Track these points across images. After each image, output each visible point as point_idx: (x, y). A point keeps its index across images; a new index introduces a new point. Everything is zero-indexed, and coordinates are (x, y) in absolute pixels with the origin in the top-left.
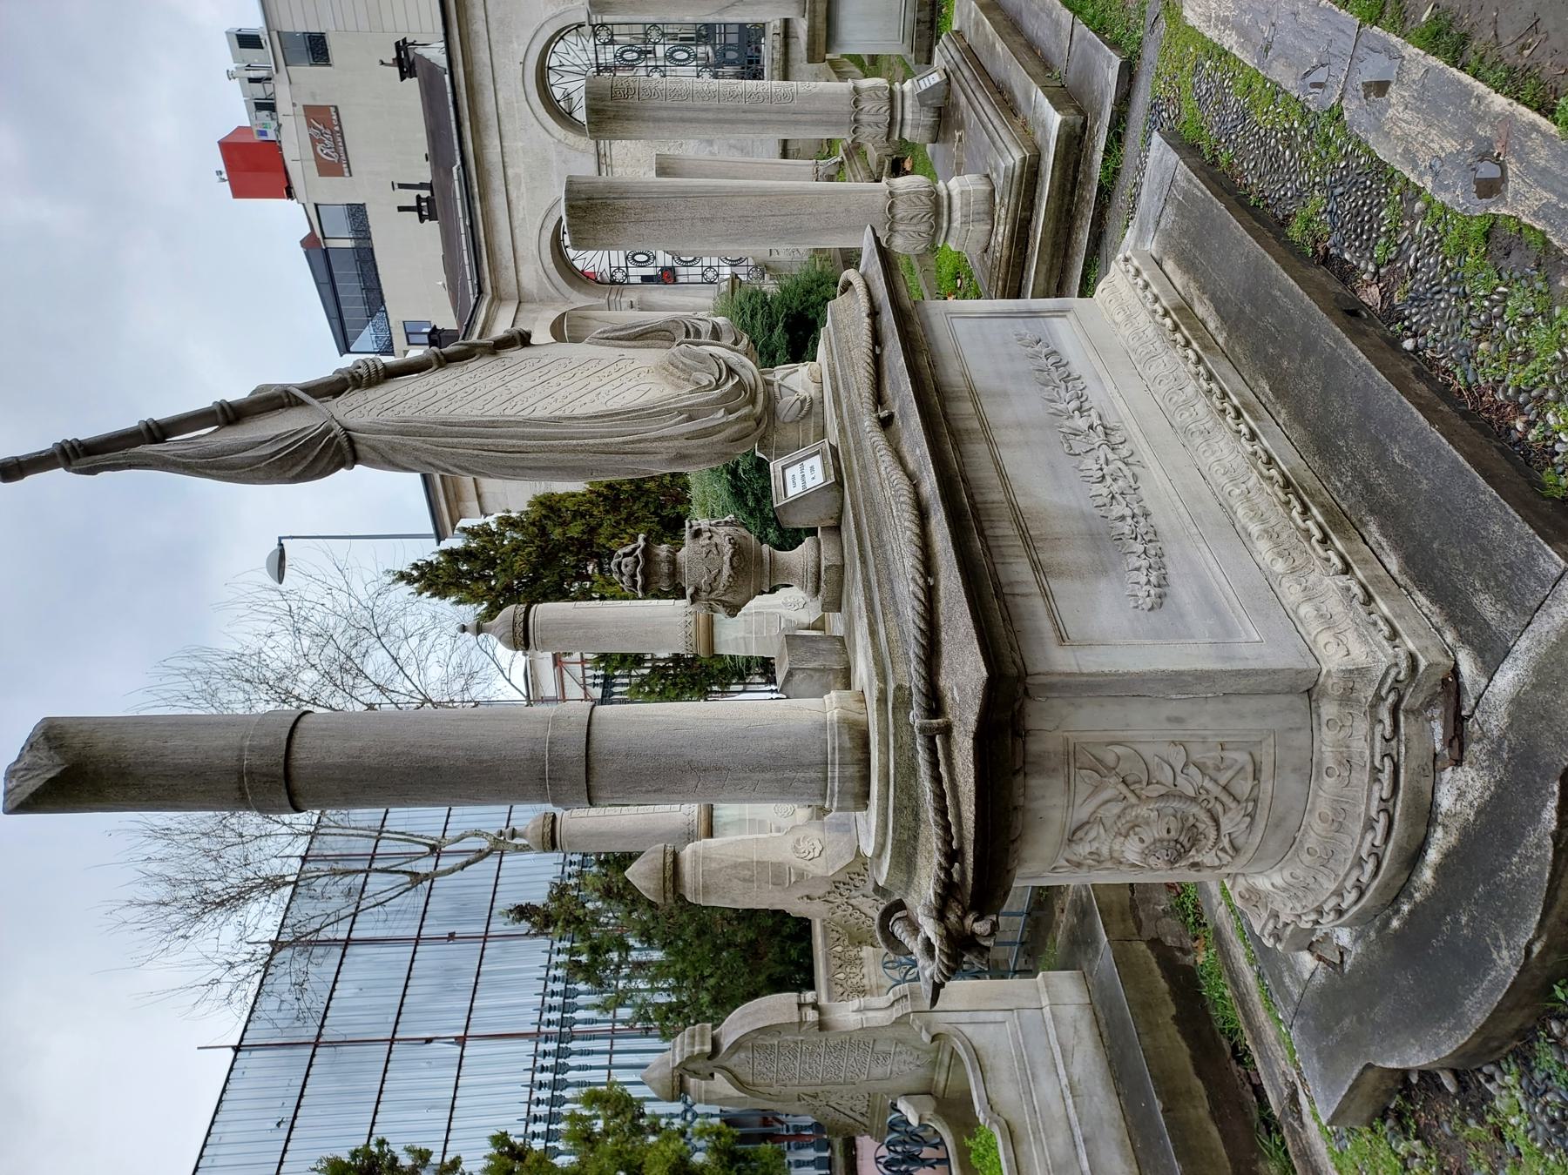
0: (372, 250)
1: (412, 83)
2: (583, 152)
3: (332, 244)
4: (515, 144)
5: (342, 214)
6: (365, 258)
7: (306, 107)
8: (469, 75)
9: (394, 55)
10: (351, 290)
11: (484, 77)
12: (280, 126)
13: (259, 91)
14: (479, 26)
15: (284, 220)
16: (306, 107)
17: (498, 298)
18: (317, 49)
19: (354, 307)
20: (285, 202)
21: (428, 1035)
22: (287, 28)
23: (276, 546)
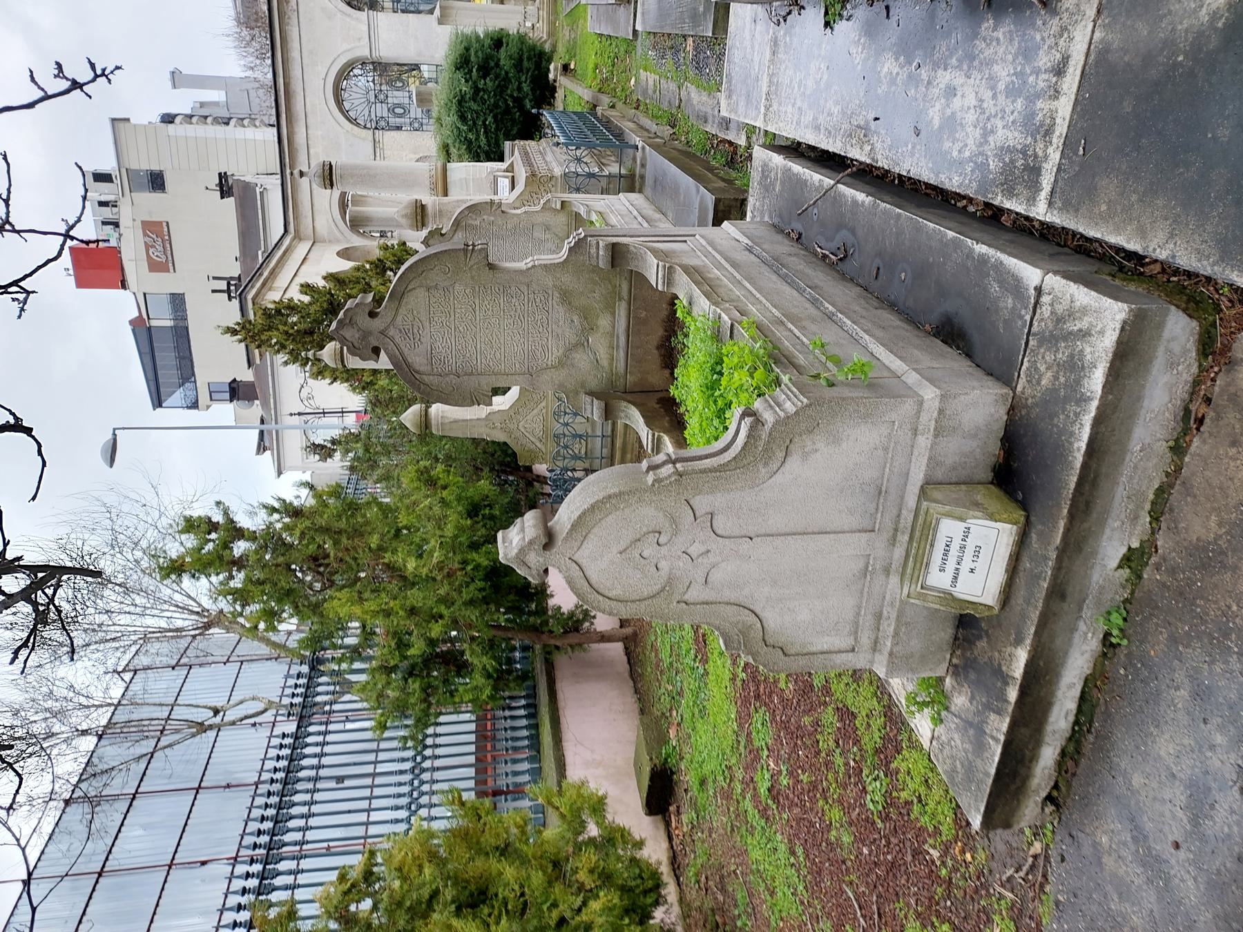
0: (187, 328)
1: (231, 201)
2: (364, 139)
3: (154, 323)
4: (315, 133)
5: (166, 300)
6: (181, 334)
7: (143, 222)
8: (286, 85)
9: (217, 181)
10: (167, 359)
11: (297, 86)
12: (120, 235)
13: (107, 213)
14: (295, 54)
15: (119, 306)
16: (143, 222)
17: (298, 237)
18: (157, 181)
19: (168, 373)
20: (119, 293)
21: (203, 859)
22: (134, 166)
23: (110, 436)
